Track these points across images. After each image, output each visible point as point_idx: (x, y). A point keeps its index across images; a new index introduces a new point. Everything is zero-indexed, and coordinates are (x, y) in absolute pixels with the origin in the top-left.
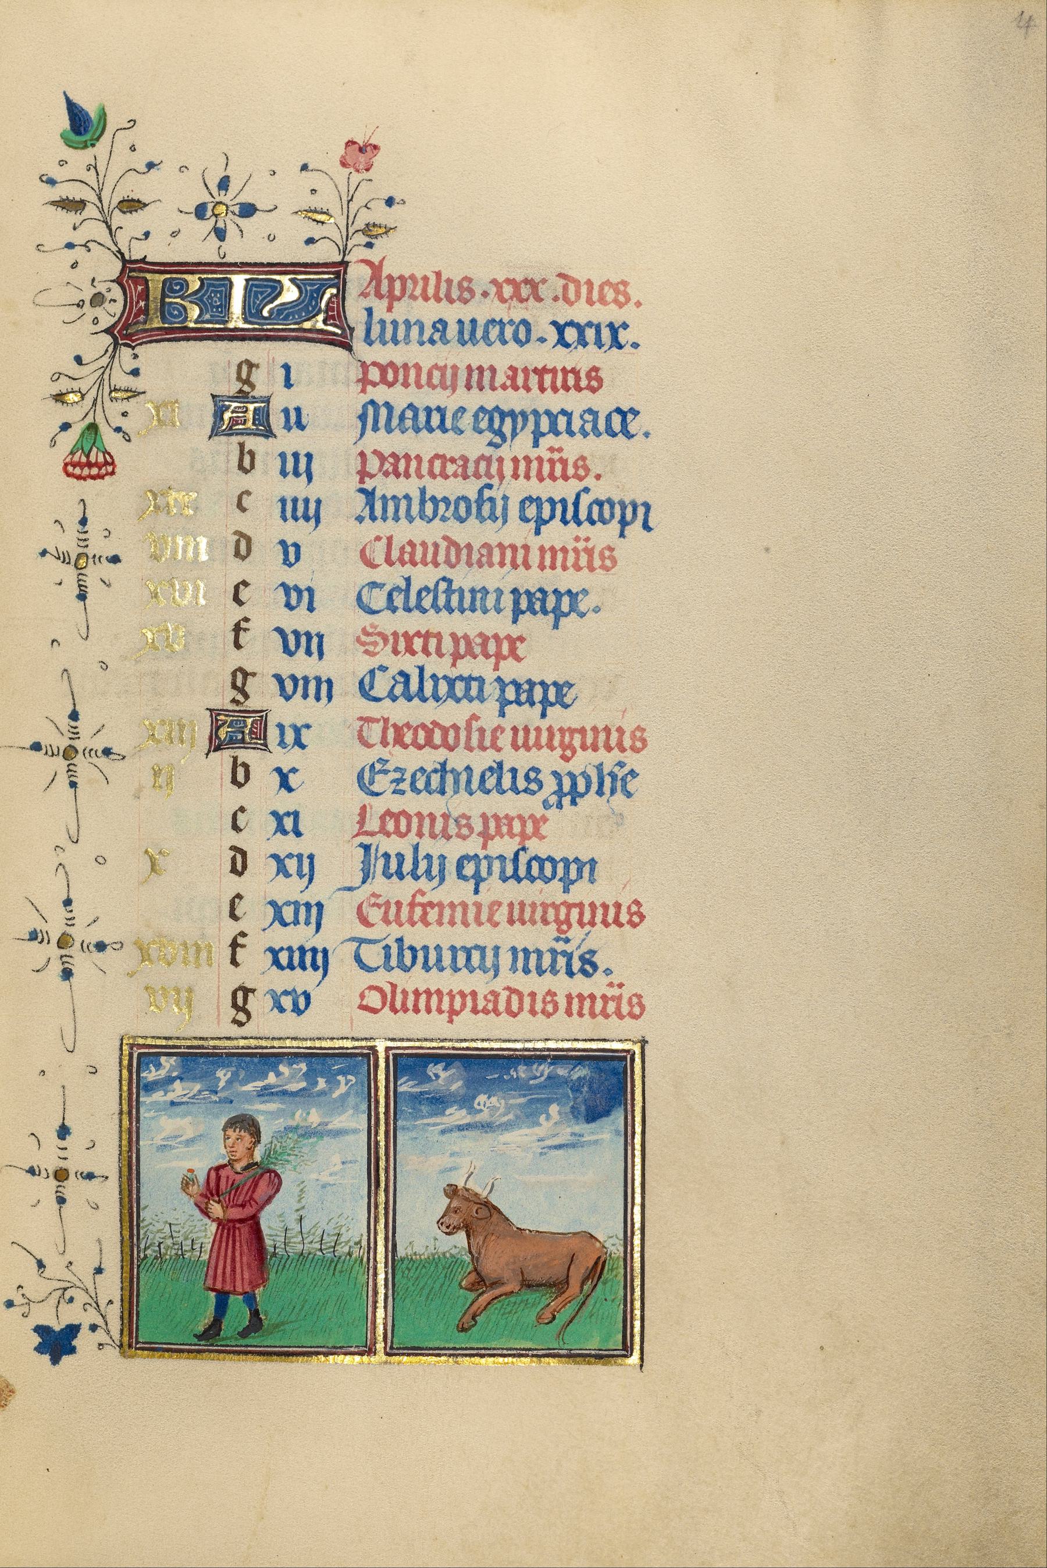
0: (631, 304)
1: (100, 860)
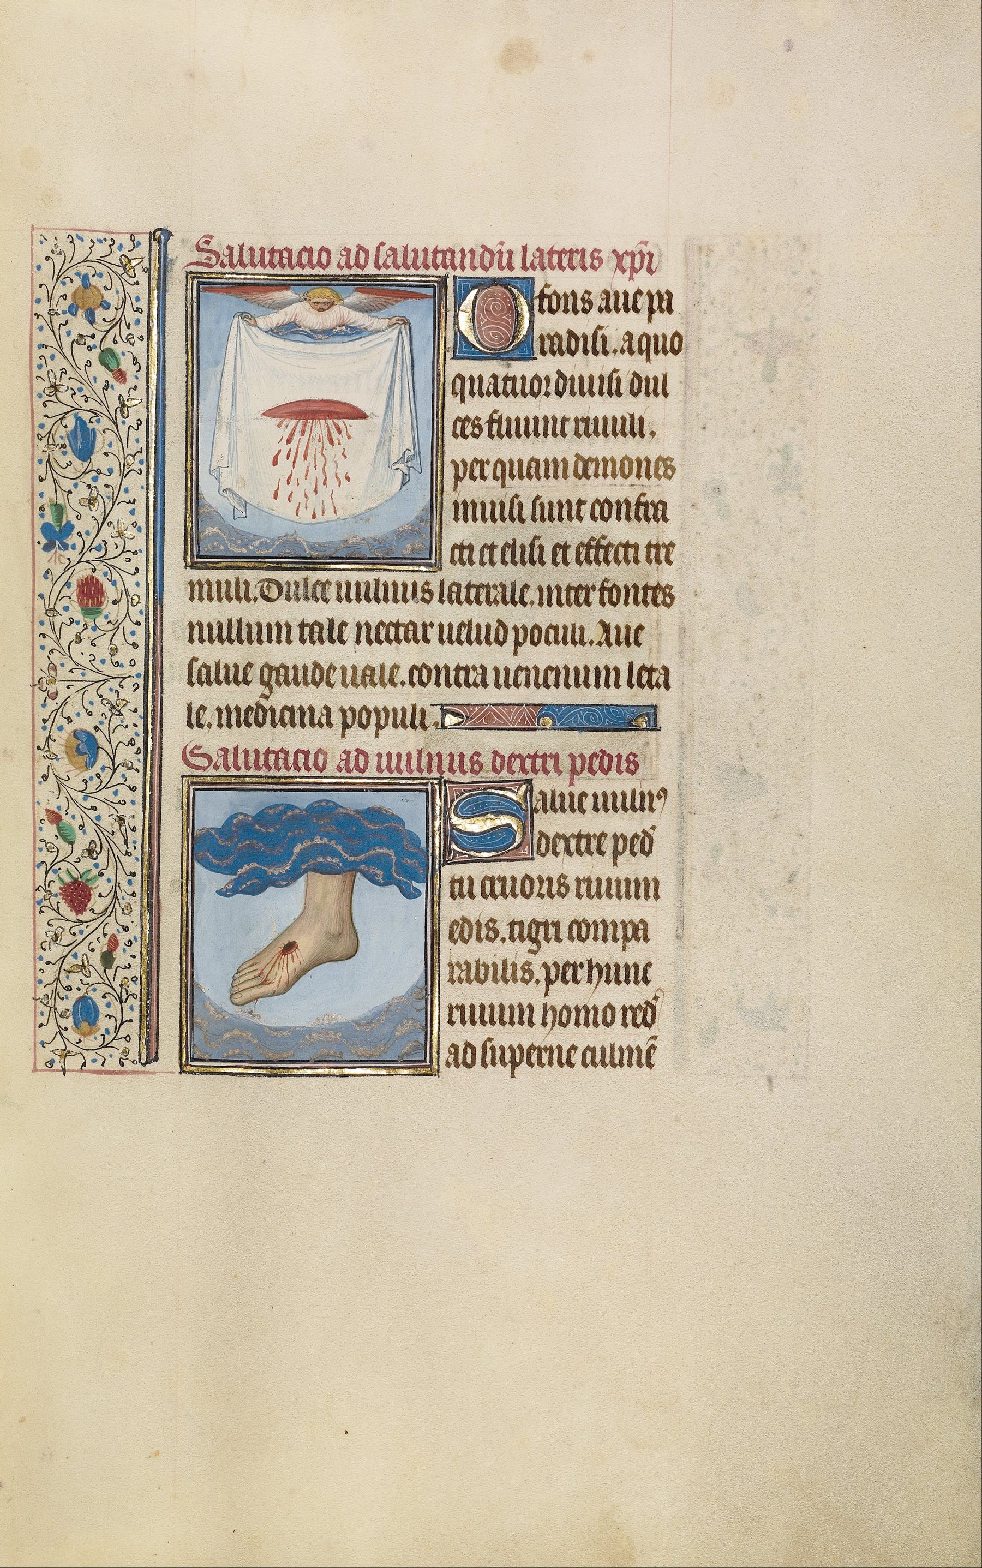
0: (499, 939)
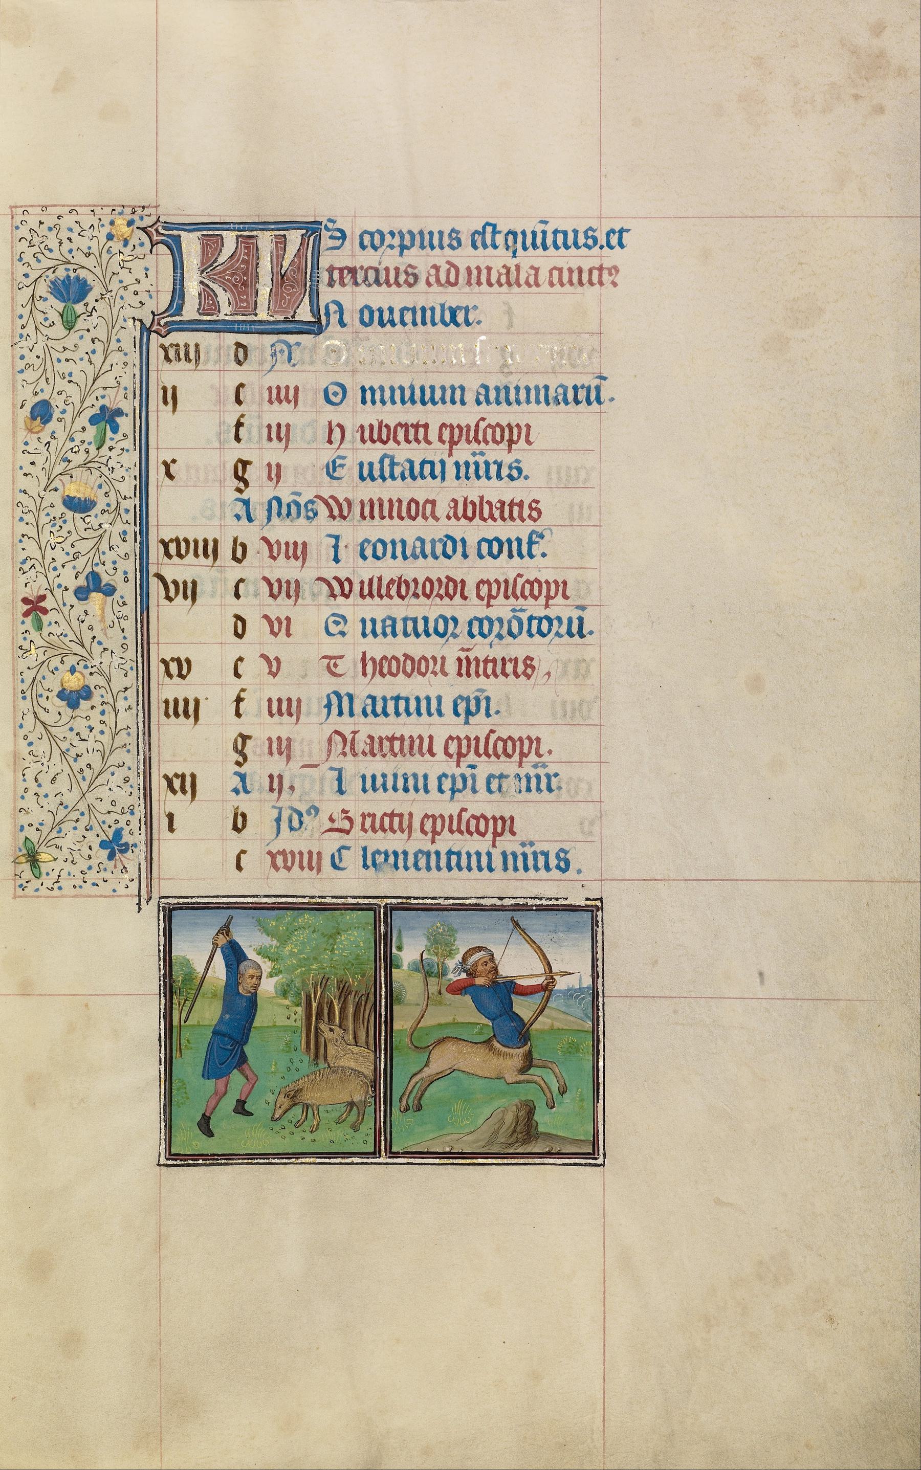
1: (113, 803)
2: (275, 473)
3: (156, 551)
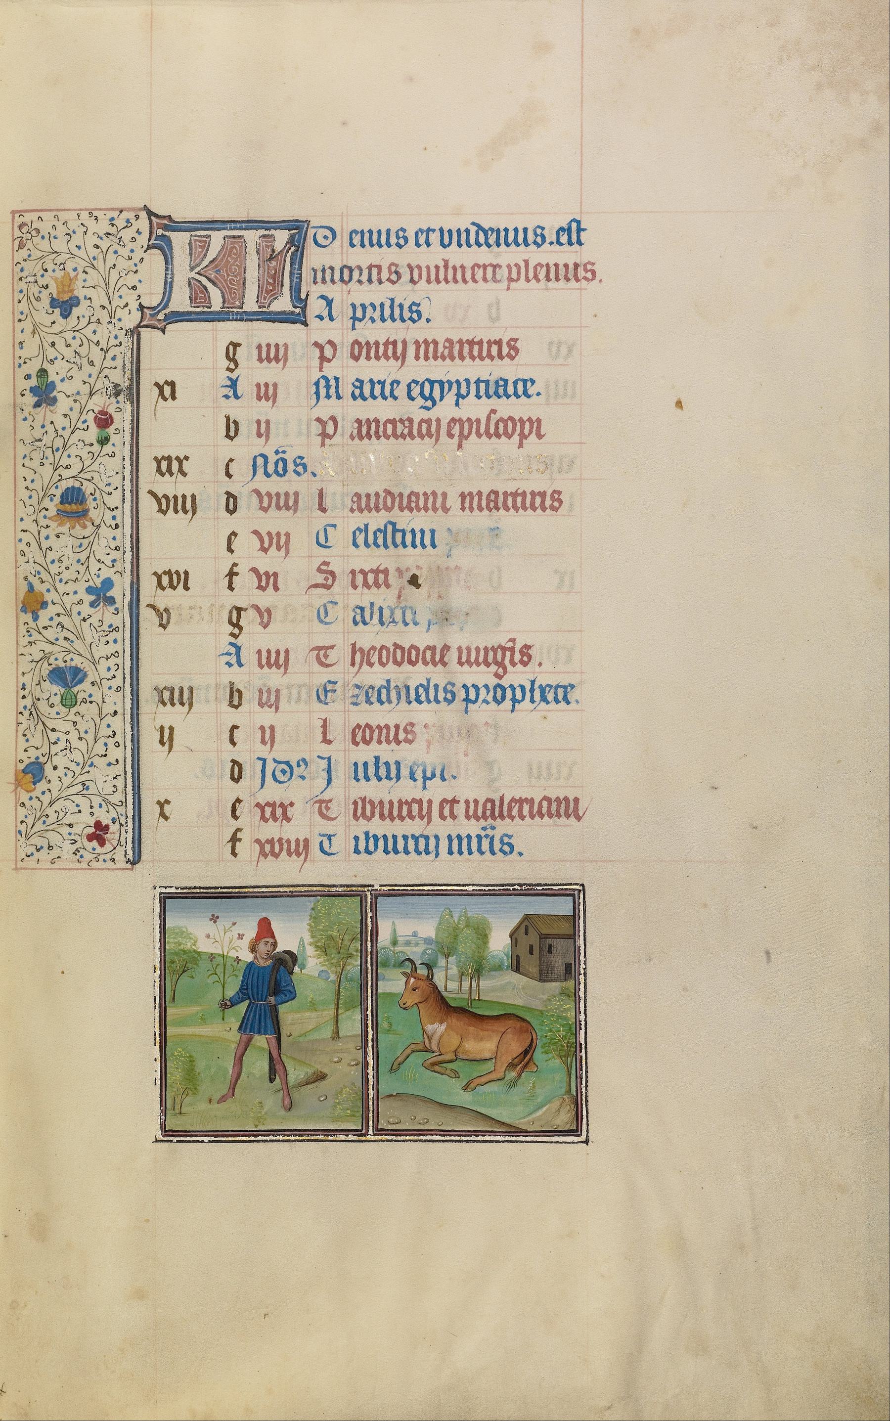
2: (263, 430)
3: (148, 584)
